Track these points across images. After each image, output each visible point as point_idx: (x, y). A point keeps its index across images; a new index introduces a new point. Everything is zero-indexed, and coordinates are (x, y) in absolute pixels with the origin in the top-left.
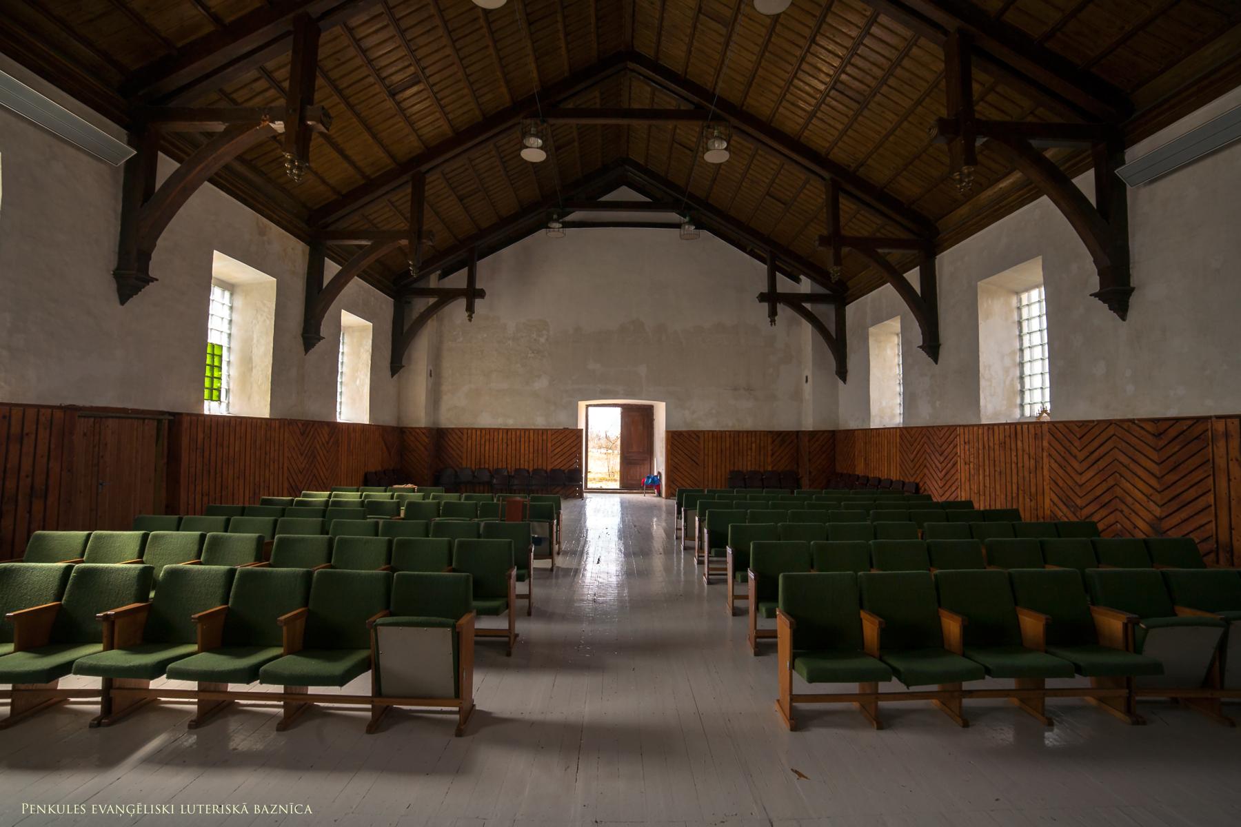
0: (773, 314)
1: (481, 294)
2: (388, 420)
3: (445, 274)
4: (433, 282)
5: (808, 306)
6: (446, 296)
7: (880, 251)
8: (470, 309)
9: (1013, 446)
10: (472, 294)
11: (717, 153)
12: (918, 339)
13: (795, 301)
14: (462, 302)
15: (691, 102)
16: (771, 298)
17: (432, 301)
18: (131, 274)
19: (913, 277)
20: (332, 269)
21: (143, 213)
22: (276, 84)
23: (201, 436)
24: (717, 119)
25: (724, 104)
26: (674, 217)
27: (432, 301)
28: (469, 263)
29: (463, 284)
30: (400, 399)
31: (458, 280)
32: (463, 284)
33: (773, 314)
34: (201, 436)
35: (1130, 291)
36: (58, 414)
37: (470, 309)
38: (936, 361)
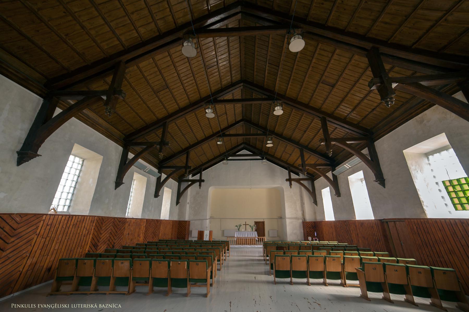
0: (291, 184)
1: (203, 181)
2: (176, 218)
3: (193, 176)
4: (190, 177)
5: (302, 182)
6: (193, 182)
7: (348, 142)
8: (200, 185)
9: (80, 226)
10: (201, 181)
11: (278, 111)
12: (334, 192)
13: (298, 181)
14: (198, 183)
15: (266, 95)
16: (290, 180)
17: (190, 183)
18: (119, 183)
19: (330, 174)
20: (131, 156)
21: (42, 127)
22: (159, 137)
23: (415, 227)
24: (277, 99)
25: (279, 95)
26: (259, 157)
27: (190, 183)
28: (200, 172)
29: (199, 178)
30: (181, 212)
31: (197, 177)
32: (199, 178)
33: (291, 184)
34: (415, 227)
35: (384, 180)
36: (134, 220)
37: (200, 185)
38: (385, 187)
